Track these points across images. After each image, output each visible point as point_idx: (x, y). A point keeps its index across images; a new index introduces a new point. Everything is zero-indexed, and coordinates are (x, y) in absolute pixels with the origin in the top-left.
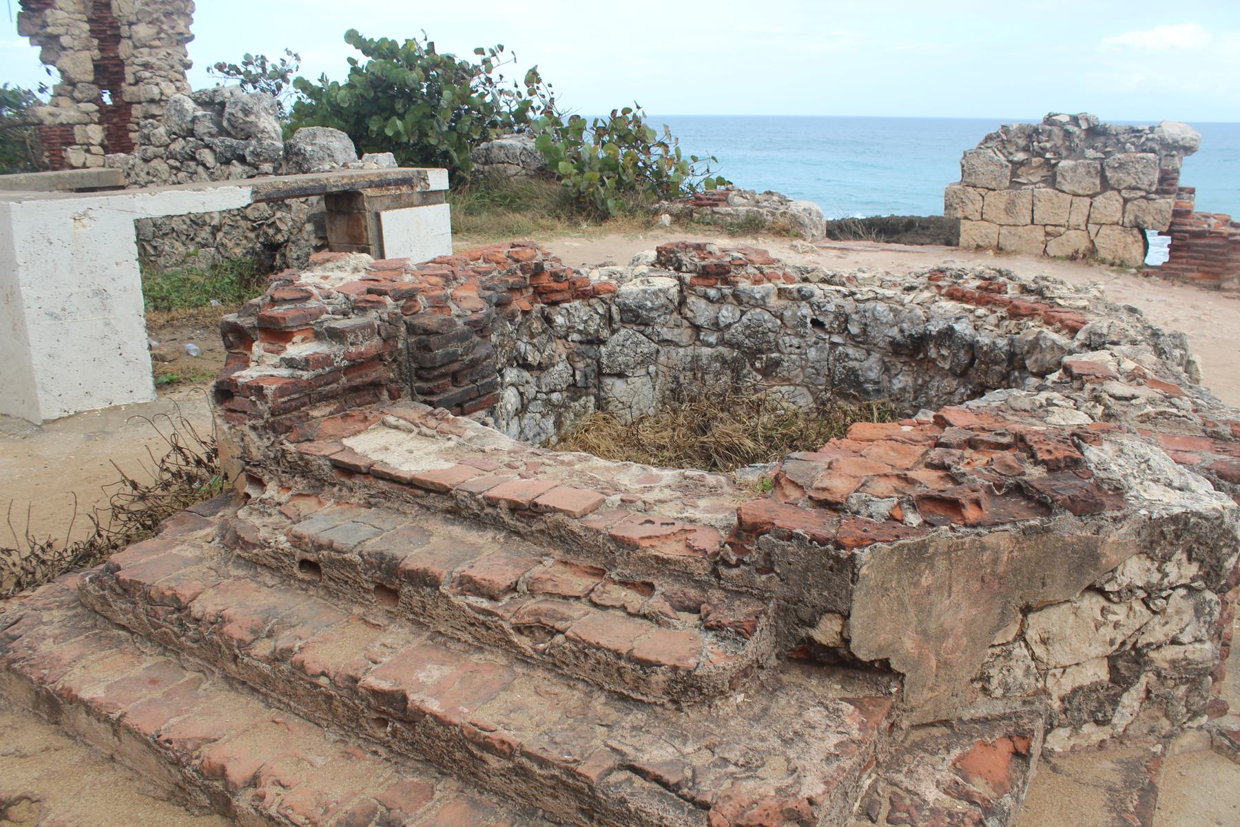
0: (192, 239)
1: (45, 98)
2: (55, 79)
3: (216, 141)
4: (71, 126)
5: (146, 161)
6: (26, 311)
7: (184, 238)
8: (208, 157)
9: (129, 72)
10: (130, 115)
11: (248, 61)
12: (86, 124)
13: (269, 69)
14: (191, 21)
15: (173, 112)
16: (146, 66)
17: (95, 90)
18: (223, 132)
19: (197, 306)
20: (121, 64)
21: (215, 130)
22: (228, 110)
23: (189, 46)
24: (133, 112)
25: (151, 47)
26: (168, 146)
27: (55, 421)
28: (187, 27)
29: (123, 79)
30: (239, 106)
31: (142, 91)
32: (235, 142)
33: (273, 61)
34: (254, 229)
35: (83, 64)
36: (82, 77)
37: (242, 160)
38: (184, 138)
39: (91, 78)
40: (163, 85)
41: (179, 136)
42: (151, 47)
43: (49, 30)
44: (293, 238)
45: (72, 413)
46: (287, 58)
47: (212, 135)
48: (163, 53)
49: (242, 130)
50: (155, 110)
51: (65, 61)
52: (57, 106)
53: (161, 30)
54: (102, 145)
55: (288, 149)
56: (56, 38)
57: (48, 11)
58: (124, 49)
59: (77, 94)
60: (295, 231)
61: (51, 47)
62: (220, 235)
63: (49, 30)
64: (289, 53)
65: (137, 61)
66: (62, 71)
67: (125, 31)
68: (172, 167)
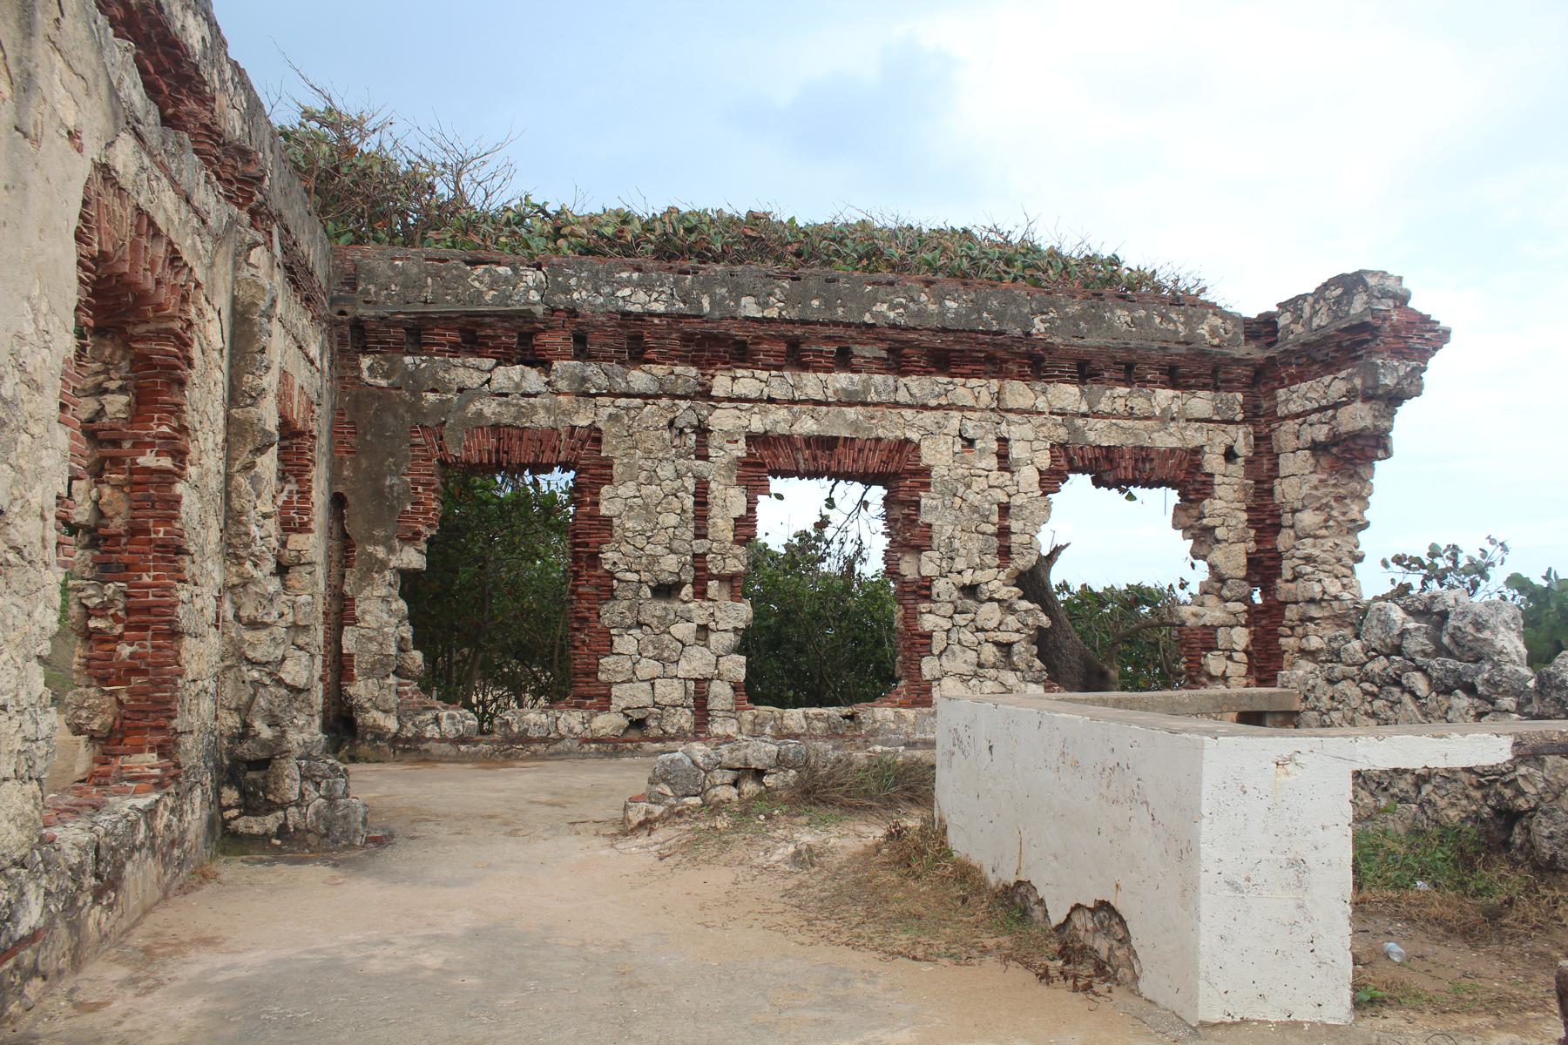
0: (1385, 789)
1: (1183, 595)
2: (1202, 572)
3: (1433, 662)
4: (1215, 628)
5: (1331, 682)
6: (1203, 875)
7: (1373, 786)
8: (1420, 683)
9: (1286, 566)
10: (1283, 616)
11: (1434, 552)
12: (1232, 627)
13: (1463, 562)
14: (1367, 505)
15: (1374, 622)
16: (1308, 559)
17: (1246, 586)
18: (1441, 650)
19: (1396, 887)
20: (1278, 557)
21: (1430, 648)
22: (1452, 622)
23: (1361, 535)
24: (1287, 613)
25: (1316, 537)
26: (1363, 665)
27: (1214, 1026)
28: (1361, 512)
29: (1280, 575)
30: (1469, 619)
31: (1301, 589)
32: (1460, 666)
33: (1470, 550)
34: (1480, 786)
35: (1233, 558)
36: (1233, 573)
37: (1470, 690)
38: (1387, 656)
39: (1243, 573)
40: (1327, 582)
41: (1380, 654)
42: (1316, 537)
43: (1205, 521)
44: (1544, 806)
45: (1237, 1019)
46: (1489, 548)
47: (1425, 654)
48: (1329, 543)
49: (1471, 649)
50: (1314, 612)
51: (1217, 556)
52: (1202, 605)
53: (1330, 517)
54: (1245, 651)
55: (1544, 683)
56: (1210, 530)
57: (1206, 502)
58: (1284, 540)
59: (1225, 592)
60: (1549, 797)
61: (1202, 538)
62: (1426, 789)
63: (1205, 521)
64: (1493, 542)
65: (1298, 554)
66: (1212, 567)
67: (1287, 519)
68: (1366, 693)
